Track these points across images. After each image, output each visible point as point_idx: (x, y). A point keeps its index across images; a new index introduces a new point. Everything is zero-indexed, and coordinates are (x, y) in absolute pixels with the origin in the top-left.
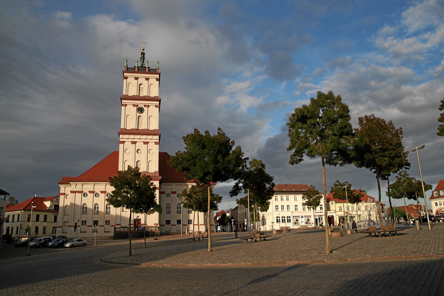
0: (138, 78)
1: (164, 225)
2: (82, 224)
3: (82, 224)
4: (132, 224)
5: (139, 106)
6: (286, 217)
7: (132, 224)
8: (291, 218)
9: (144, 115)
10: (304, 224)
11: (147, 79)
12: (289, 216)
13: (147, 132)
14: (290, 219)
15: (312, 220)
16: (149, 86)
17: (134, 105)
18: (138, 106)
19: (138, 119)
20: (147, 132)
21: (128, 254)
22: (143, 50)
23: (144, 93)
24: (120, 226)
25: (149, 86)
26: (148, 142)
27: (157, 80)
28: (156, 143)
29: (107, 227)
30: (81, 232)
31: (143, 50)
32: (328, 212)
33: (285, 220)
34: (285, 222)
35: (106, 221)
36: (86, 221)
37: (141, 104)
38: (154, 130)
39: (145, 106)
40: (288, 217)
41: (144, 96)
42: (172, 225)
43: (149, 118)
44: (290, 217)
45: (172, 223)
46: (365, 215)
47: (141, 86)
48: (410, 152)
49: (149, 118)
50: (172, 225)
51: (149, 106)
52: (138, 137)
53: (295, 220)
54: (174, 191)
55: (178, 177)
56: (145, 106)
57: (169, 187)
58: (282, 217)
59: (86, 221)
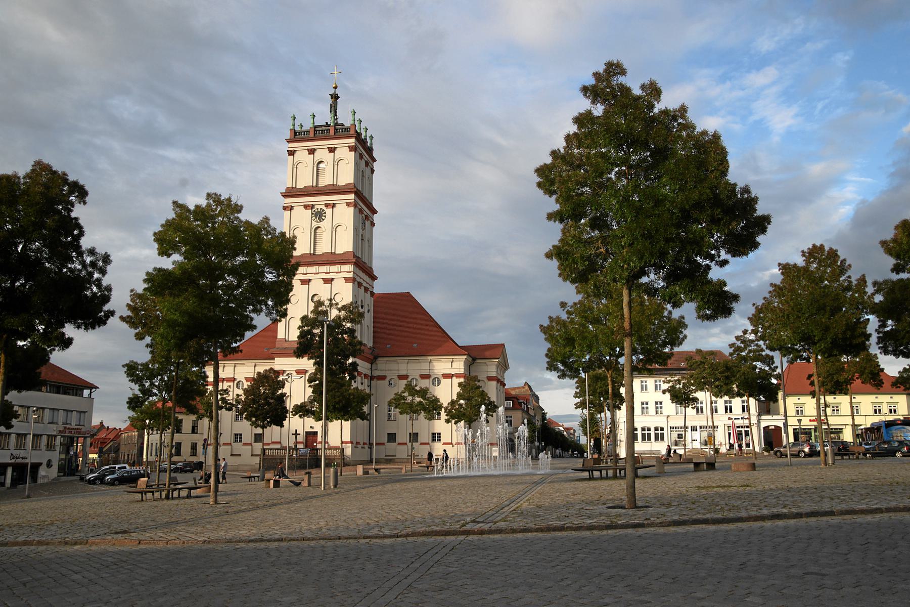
0: (315, 150)
1: (383, 444)
2: (236, 441)
3: (236, 441)
4: (300, 443)
5: (316, 207)
6: (653, 429)
7: (300, 443)
8: (665, 432)
9: (326, 224)
10: (697, 445)
11: (332, 150)
12: (660, 425)
13: (332, 259)
14: (662, 435)
15: (721, 437)
16: (336, 163)
17: (306, 207)
18: (313, 206)
19: (315, 233)
20: (332, 259)
21: (625, 498)
22: (335, 88)
23: (326, 180)
24: (278, 446)
25: (336, 163)
26: (332, 279)
27: (350, 151)
28: (347, 280)
29: (237, 446)
30: (232, 455)
31: (335, 88)
32: (763, 417)
33: (649, 435)
34: (649, 439)
35: (236, 435)
36: (241, 435)
37: (319, 201)
38: (345, 253)
39: (327, 206)
40: (656, 429)
41: (326, 186)
42: (399, 444)
43: (335, 229)
44: (662, 429)
45: (399, 439)
46: (334, 439)
47: (321, 165)
48: (117, 315)
49: (335, 229)
50: (399, 444)
51: (334, 206)
52: (334, 268)
53: (675, 435)
54: (404, 373)
55: (415, 345)
56: (327, 206)
57: (393, 366)
58: (643, 429)
59: (241, 435)
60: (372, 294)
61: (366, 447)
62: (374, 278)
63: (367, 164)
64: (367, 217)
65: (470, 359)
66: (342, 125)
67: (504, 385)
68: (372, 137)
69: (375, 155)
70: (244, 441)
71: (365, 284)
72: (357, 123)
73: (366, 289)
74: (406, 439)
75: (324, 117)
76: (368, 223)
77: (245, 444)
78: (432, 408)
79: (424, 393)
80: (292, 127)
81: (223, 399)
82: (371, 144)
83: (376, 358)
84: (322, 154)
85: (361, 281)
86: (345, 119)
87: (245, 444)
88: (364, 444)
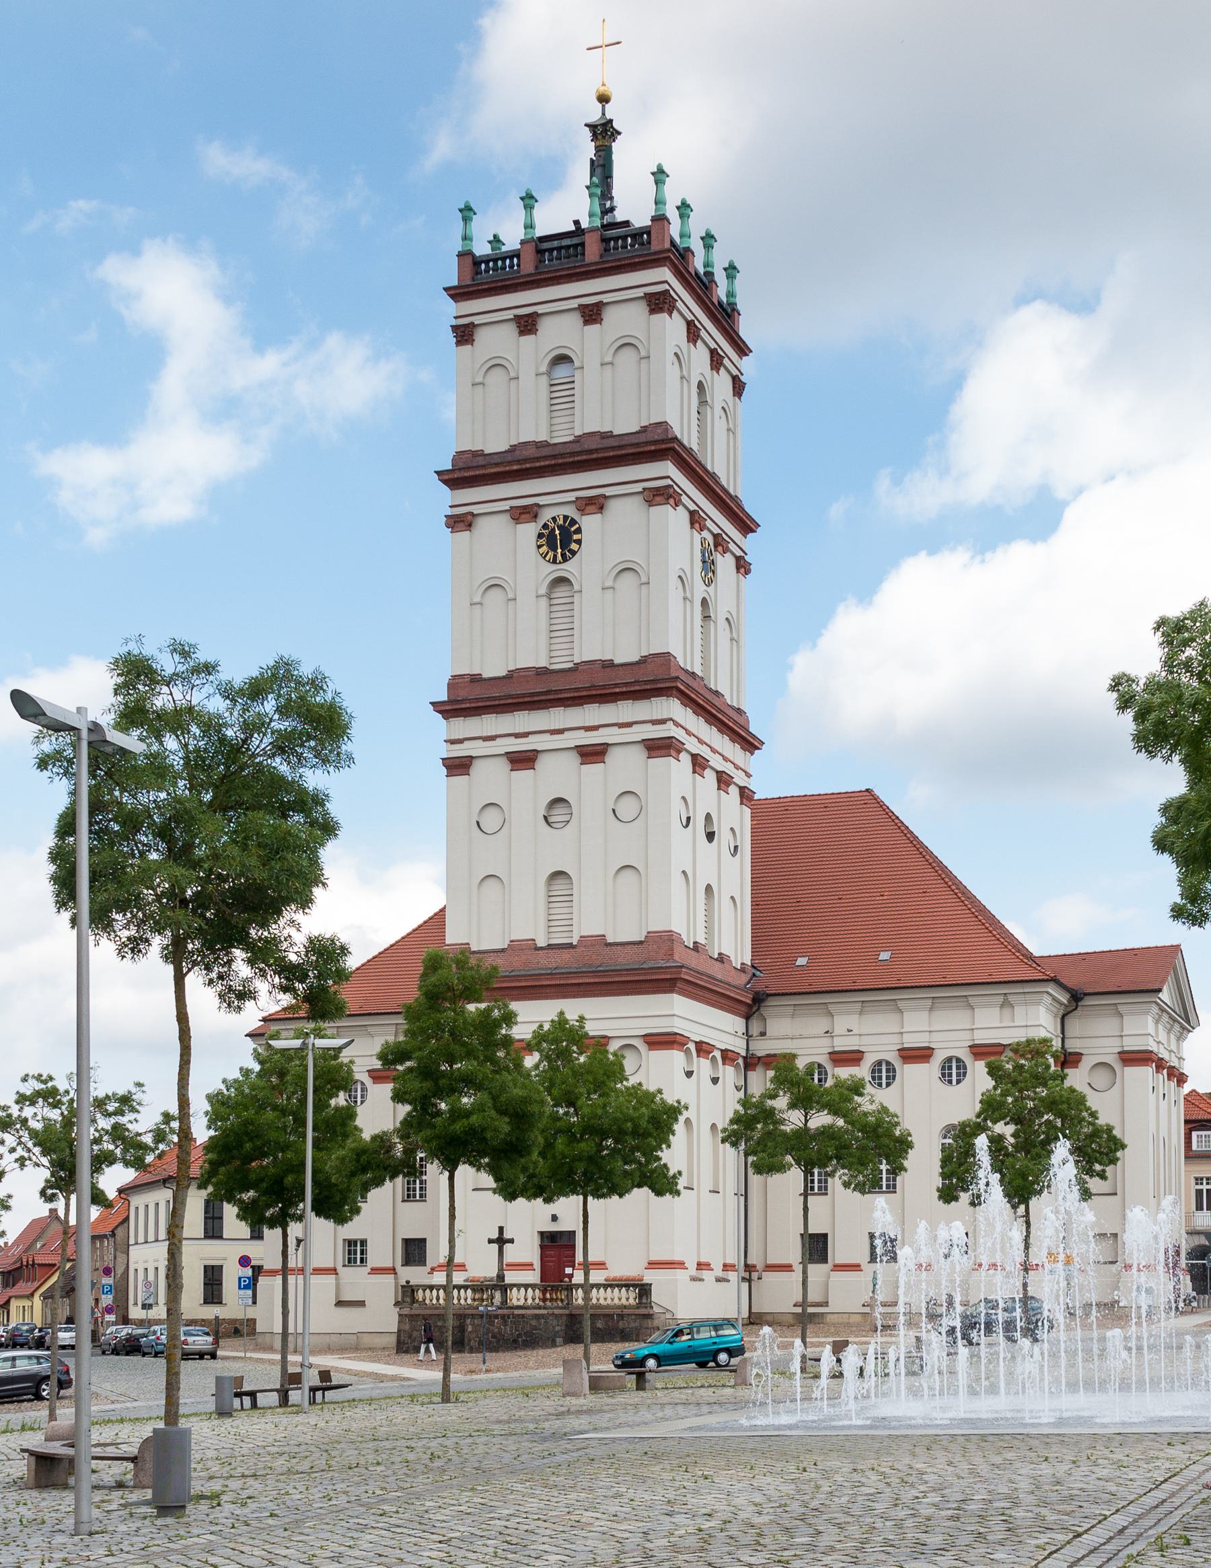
2: (351, 1262)
3: (351, 1262)
30: (340, 1303)
31: (604, 99)
35: (407, 1242)
36: (363, 1243)
37: (556, 492)
50: (839, 1267)
59: (363, 1243)
60: (746, 795)
61: (733, 1276)
62: (750, 744)
63: (716, 360)
64: (720, 542)
65: (1064, 998)
66: (626, 223)
67: (1181, 1079)
68: (731, 270)
69: (745, 329)
70: (374, 1259)
71: (716, 762)
72: (672, 214)
73: (723, 780)
74: (793, 1253)
75: (566, 209)
76: (725, 564)
77: (375, 1271)
78: (626, 1133)
79: (841, 1099)
80: (459, 246)
81: (118, 1133)
82: (731, 294)
83: (759, 999)
84: (560, 331)
85: (704, 752)
86: (633, 205)
87: (375, 1271)
88: (726, 1267)
